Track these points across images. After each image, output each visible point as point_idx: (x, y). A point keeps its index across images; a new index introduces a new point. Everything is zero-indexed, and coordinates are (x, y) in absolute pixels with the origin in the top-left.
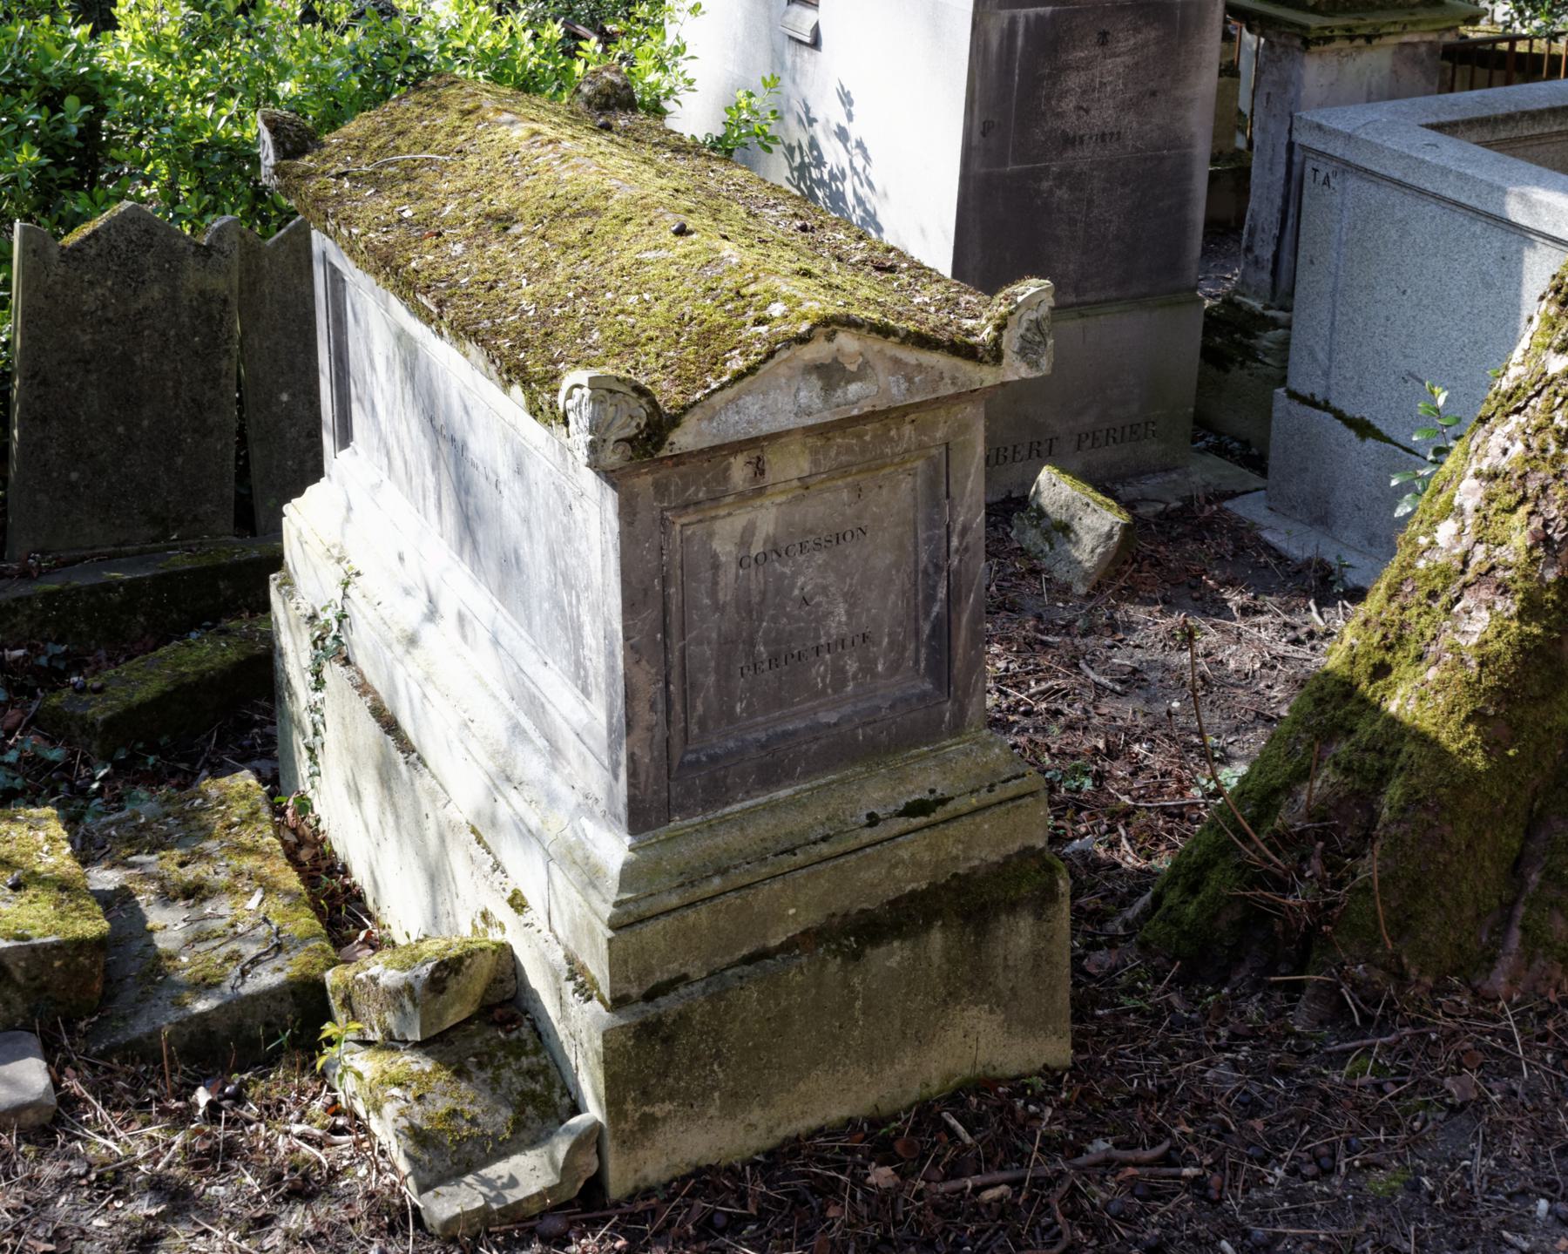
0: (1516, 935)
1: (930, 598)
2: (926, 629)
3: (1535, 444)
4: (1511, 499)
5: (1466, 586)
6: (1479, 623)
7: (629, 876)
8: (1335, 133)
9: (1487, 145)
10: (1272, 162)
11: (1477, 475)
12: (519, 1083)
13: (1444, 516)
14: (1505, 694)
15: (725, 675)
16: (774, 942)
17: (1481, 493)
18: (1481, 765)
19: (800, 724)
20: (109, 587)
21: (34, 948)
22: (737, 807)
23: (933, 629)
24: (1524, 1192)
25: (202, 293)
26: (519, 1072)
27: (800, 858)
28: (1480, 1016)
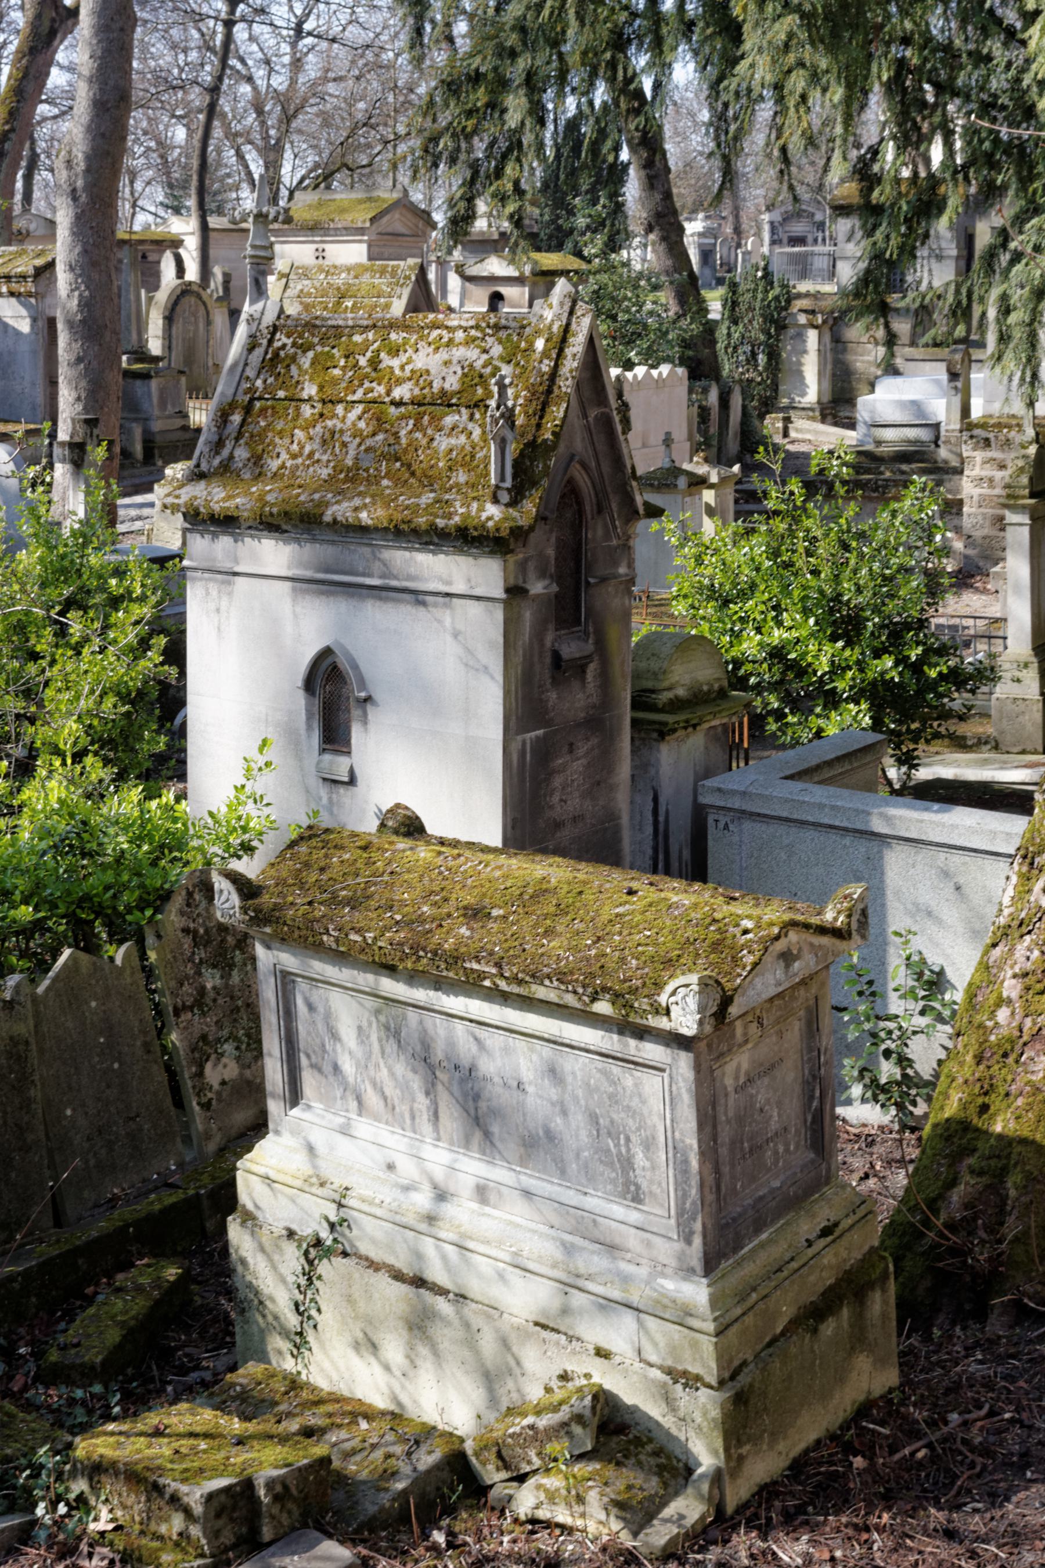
1: (812, 1097)
2: (809, 1118)
8: (733, 793)
9: (819, 783)
11: (1015, 976)
12: (653, 1461)
15: (733, 1166)
16: (778, 1331)
17: (1019, 987)
20: (11, 1278)
21: (300, 1469)
22: (746, 1249)
25: (11, 1038)
26: (649, 1455)
27: (786, 1273)
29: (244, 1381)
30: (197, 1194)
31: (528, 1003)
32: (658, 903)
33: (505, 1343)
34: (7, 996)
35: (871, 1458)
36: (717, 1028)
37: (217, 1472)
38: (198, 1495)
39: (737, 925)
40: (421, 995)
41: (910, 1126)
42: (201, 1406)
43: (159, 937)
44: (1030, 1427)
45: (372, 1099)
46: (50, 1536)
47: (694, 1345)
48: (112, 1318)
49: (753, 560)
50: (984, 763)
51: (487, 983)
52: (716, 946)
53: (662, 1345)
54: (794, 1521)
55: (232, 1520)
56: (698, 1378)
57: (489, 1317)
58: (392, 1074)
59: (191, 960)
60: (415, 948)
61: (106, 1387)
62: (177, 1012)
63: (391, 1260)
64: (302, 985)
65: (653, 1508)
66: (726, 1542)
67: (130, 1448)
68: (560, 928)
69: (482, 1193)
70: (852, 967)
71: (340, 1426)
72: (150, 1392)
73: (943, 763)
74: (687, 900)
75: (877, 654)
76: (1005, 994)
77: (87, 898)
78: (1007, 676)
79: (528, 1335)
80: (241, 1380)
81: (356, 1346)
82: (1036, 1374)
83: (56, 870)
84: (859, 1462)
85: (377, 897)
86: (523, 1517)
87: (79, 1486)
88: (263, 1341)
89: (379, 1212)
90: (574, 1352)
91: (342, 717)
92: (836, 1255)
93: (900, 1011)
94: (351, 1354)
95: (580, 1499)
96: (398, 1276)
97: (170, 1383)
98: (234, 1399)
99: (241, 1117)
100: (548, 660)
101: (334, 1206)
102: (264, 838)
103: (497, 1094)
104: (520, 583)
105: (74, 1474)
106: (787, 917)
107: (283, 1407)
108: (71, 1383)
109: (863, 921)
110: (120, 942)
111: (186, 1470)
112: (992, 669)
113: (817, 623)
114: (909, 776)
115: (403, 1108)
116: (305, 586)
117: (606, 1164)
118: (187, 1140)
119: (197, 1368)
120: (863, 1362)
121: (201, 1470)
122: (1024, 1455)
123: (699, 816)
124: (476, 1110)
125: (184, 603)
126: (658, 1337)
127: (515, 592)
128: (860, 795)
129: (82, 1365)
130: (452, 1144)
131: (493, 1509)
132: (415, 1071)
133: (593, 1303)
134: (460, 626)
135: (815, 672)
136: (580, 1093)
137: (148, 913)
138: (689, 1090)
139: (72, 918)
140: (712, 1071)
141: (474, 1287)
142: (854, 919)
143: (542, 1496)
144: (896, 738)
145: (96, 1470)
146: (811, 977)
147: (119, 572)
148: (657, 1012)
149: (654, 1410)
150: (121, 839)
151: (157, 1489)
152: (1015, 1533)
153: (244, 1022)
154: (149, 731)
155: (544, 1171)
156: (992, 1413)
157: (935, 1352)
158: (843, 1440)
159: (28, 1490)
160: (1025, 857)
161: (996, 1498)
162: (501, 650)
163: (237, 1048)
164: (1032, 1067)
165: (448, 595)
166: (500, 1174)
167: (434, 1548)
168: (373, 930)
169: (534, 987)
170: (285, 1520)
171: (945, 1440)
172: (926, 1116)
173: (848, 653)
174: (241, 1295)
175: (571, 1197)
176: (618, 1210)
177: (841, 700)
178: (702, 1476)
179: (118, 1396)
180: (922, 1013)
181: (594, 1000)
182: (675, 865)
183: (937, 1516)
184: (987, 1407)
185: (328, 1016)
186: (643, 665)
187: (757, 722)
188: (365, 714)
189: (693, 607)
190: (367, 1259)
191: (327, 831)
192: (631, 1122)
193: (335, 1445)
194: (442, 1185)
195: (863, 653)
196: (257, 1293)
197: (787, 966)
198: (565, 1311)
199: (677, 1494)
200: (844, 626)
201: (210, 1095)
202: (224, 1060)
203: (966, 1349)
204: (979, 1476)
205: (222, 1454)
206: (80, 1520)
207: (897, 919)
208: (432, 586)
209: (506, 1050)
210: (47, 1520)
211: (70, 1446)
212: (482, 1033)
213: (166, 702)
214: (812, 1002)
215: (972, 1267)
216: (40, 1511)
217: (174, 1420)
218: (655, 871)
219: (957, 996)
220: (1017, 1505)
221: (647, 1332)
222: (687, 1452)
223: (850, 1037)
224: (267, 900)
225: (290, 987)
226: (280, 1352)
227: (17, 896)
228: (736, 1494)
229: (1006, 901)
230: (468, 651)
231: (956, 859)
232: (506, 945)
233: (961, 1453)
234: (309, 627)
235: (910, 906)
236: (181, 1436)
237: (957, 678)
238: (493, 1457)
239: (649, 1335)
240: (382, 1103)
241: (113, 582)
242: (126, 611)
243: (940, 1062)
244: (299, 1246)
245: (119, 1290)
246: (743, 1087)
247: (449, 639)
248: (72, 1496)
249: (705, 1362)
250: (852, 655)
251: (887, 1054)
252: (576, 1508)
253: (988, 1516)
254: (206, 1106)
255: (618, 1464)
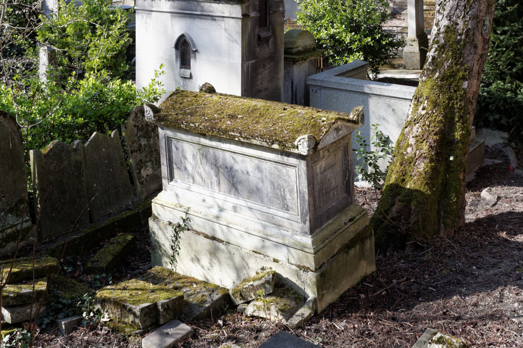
0: (442, 225)
1: (346, 176)
3: (423, 128)
4: (421, 140)
5: (417, 159)
6: (422, 166)
7: (313, 243)
8: (318, 80)
10: (287, 91)
11: (413, 137)
12: (293, 296)
13: (408, 147)
14: (431, 178)
16: (335, 253)
18: (430, 193)
19: (331, 206)
20: (75, 240)
21: (173, 300)
22: (324, 226)
23: (346, 183)
24: (469, 267)
25: (76, 161)
26: (292, 294)
27: (338, 233)
28: (442, 241)
29: (154, 272)
30: (138, 212)
31: (250, 146)
32: (294, 113)
33: (243, 259)
34: (75, 147)
35: (367, 295)
36: (314, 153)
37: (144, 301)
38: (138, 309)
39: (321, 119)
40: (214, 144)
41: (378, 188)
42: (140, 280)
43: (126, 128)
44: (420, 284)
45: (198, 178)
46: (87, 323)
47: (307, 257)
48: (109, 252)
49: (324, 7)
50: (401, 72)
51: (236, 139)
52: (313, 126)
53: (296, 257)
54: (341, 316)
55: (150, 317)
56: (308, 268)
57: (237, 249)
58: (204, 170)
59: (137, 135)
60: (212, 128)
61: (107, 275)
62: (132, 153)
63: (204, 231)
64: (174, 141)
65: (293, 311)
66: (318, 322)
67: (115, 294)
68: (261, 121)
69: (235, 209)
70: (358, 136)
71: (186, 286)
72: (122, 276)
73: (387, 73)
74: (304, 112)
75: (366, 37)
76: (410, 143)
77: (102, 115)
78: (408, 44)
79: (251, 255)
80: (153, 272)
81: (192, 260)
82: (421, 267)
83: (91, 106)
84: (363, 296)
85: (199, 112)
86: (249, 315)
87: (98, 307)
88: (161, 259)
89: (200, 215)
90: (266, 260)
91: (188, 57)
92: (354, 228)
93: (375, 151)
94: (191, 263)
95: (269, 309)
96: (206, 237)
97: (129, 273)
98: (150, 278)
99: (153, 187)
100: (256, 38)
101: (185, 214)
102: (161, 96)
103: (241, 176)
104: (247, 13)
105: (96, 303)
106: (337, 116)
107: (167, 280)
108: (95, 274)
109: (363, 118)
110: (113, 130)
111: (134, 301)
112: (403, 42)
113: (345, 27)
114: (376, 76)
115: (208, 181)
116: (175, 15)
117: (277, 198)
118: (135, 194)
119: (138, 268)
120: (364, 263)
121: (139, 301)
122: (418, 293)
123: (307, 88)
124: (233, 181)
125: (135, 24)
126: (295, 255)
127: (245, 16)
128: (360, 81)
129: (99, 267)
130: (225, 193)
131: (239, 313)
132: (212, 169)
133: (272, 244)
134: (227, 27)
135: (345, 43)
136: (268, 175)
137: (122, 120)
138: (305, 173)
139: (96, 122)
140: (312, 167)
141: (232, 240)
142: (360, 117)
143: (255, 308)
144: (372, 64)
145: (104, 301)
146: (345, 136)
147: (113, 13)
148: (294, 148)
149: (293, 279)
150: (113, 96)
151: (124, 307)
152: (416, 318)
153: (155, 156)
154: (123, 63)
155: (256, 201)
156: (407, 280)
157: (388, 260)
158: (357, 289)
159: (80, 308)
160: (416, 99)
161: (409, 307)
162: (241, 34)
163: (152, 164)
164: (419, 167)
165: (223, 17)
166: (241, 202)
167: (219, 325)
168: (198, 123)
169: (252, 140)
170: (168, 317)
171: (391, 288)
172: (383, 184)
173: (356, 36)
174: (153, 244)
175: (265, 209)
176: (281, 214)
177: (354, 52)
178: (310, 301)
179: (111, 278)
180: (382, 151)
181: (272, 144)
182: (298, 99)
183: (389, 313)
184: (406, 277)
185: (183, 151)
186: (288, 40)
187: (326, 59)
188: (195, 56)
189: (304, 22)
190: (196, 231)
191: (182, 91)
192: (285, 184)
193: (185, 292)
194: (221, 206)
195: (361, 36)
196: (158, 243)
197: (337, 133)
198: (263, 247)
199: (301, 307)
200: (354, 27)
201: (143, 180)
202: (148, 168)
203: (398, 259)
204: (403, 300)
205: (147, 295)
206: (98, 318)
207: (373, 120)
208: (217, 14)
209: (243, 161)
210: (87, 318)
211: (95, 294)
212: (235, 156)
213: (128, 53)
214: (346, 145)
215: (400, 232)
216: (84, 315)
217: (130, 284)
218: (292, 103)
219: (393, 145)
220: (416, 309)
221: (291, 253)
222: (305, 293)
223: (358, 159)
224: (162, 113)
225: (170, 142)
226: (166, 263)
227: (78, 115)
228: (322, 306)
229: (410, 113)
230: (230, 35)
231: (393, 101)
232: (243, 127)
233: (397, 293)
234: (178, 28)
235: (377, 116)
236: (132, 290)
237: (392, 44)
238: (239, 295)
239: (292, 255)
240: (201, 180)
241: (111, 16)
242: (115, 25)
243: (388, 167)
244: (173, 227)
245: (112, 243)
246: (323, 172)
247: (223, 31)
248: (95, 310)
249: (311, 263)
250: (357, 37)
251: (370, 164)
252: (267, 312)
253: (407, 313)
254: (142, 183)
255: (281, 297)
